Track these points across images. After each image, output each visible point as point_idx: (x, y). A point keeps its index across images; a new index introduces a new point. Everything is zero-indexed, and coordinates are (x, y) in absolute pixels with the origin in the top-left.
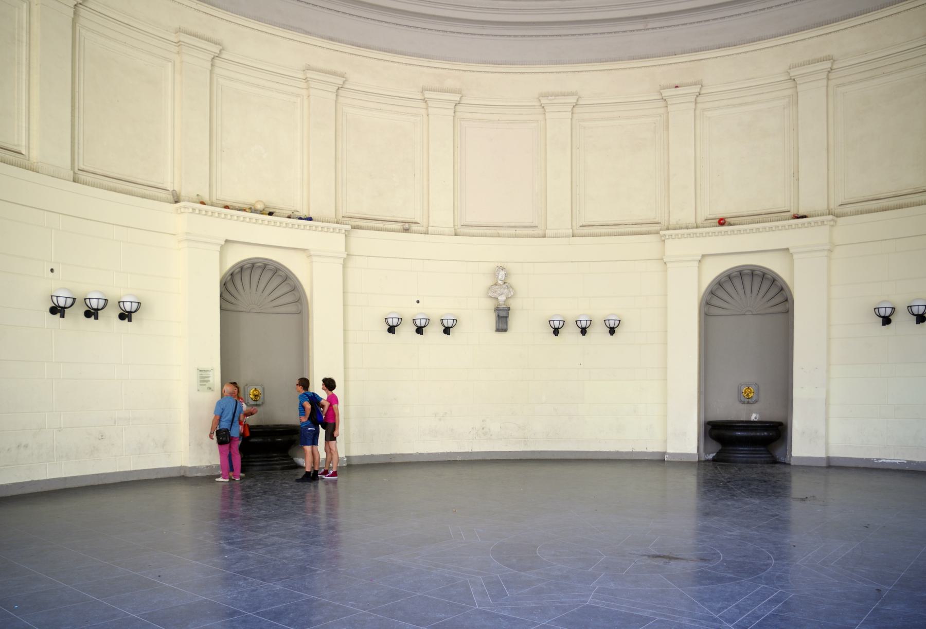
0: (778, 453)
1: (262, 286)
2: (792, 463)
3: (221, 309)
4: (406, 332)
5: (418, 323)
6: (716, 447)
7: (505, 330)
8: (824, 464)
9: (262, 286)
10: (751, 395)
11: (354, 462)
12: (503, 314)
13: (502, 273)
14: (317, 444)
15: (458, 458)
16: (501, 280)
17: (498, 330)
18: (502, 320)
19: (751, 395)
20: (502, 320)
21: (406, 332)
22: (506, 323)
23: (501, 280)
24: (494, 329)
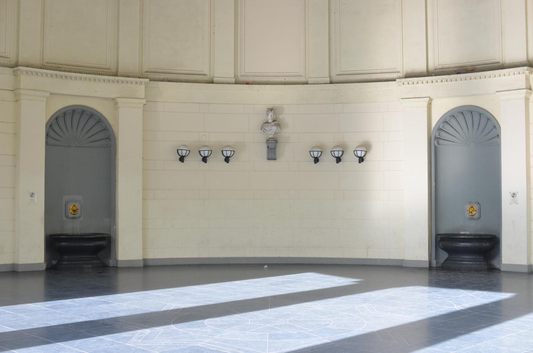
0: (495, 263)
1: (81, 126)
2: (502, 269)
3: (47, 143)
4: (328, 160)
5: (359, 154)
6: (444, 255)
7: (275, 159)
8: (526, 270)
9: (81, 126)
10: (474, 213)
11: (150, 263)
12: (272, 146)
13: (271, 114)
14: (437, 282)
15: (232, 262)
16: (274, 118)
17: (269, 159)
18: (272, 149)
19: (474, 213)
20: (272, 149)
21: (328, 160)
22: (275, 153)
23: (274, 118)
24: (266, 157)
